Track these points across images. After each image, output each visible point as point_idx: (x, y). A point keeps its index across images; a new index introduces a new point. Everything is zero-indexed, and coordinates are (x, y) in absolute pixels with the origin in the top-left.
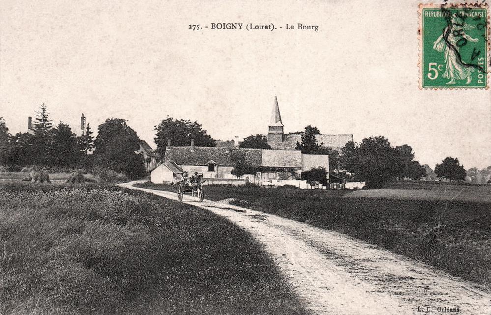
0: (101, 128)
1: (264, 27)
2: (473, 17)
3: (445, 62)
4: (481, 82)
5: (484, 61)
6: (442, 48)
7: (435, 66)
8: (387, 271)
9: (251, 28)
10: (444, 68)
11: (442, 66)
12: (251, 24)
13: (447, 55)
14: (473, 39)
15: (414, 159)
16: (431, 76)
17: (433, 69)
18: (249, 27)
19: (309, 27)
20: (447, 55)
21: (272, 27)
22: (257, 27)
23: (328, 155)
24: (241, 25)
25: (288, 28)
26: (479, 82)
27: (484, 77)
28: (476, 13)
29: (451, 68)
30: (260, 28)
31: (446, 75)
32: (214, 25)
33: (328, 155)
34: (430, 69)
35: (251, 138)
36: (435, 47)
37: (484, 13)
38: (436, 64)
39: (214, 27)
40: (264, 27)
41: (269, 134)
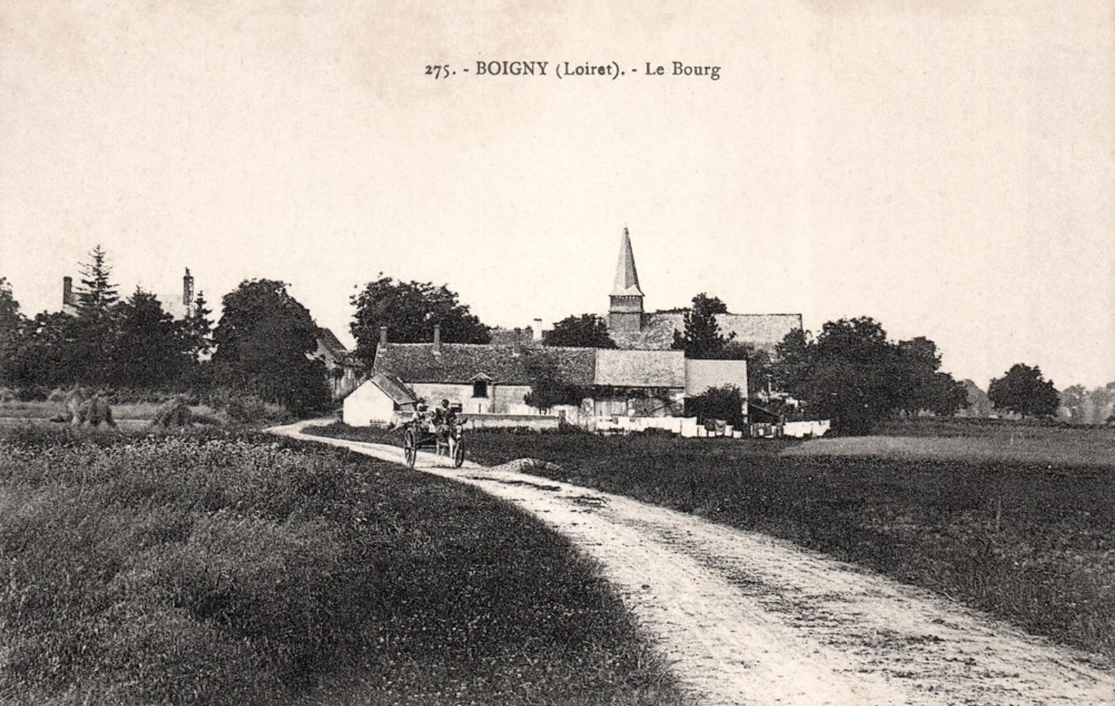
1: (596, 71)
9: (567, 73)
18: (562, 71)
19: (698, 71)
24: (543, 65)
30: (587, 73)
32: (482, 65)
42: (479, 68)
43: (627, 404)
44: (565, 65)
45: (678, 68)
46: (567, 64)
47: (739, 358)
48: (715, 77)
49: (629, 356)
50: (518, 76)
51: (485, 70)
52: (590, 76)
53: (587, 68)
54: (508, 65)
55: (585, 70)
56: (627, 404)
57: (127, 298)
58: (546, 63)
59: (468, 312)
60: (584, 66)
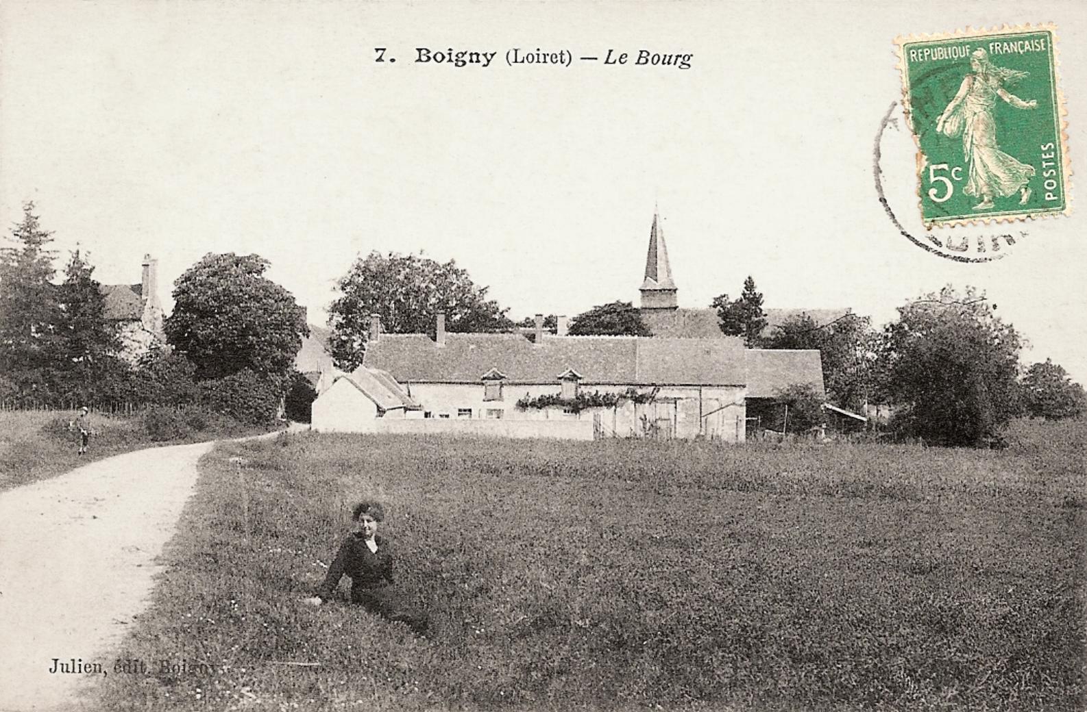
1: (548, 59)
2: (1021, 52)
3: (966, 160)
4: (1052, 198)
5: (1055, 150)
6: (955, 129)
7: (944, 169)
9: (516, 62)
10: (965, 175)
11: (960, 169)
13: (968, 145)
14: (1024, 103)
16: (935, 195)
17: (937, 179)
18: (512, 58)
19: (667, 60)
20: (968, 145)
21: (566, 57)
22: (532, 58)
26: (1047, 199)
27: (1058, 184)
28: (1005, 44)
29: (980, 171)
31: (971, 189)
32: (644, 54)
34: (933, 179)
36: (939, 129)
37: (1045, 42)
38: (945, 166)
41: (62, 664)
42: (640, 57)
44: (514, 52)
45: (644, 58)
46: (516, 50)
47: (812, 344)
48: (460, 64)
49: (792, 365)
51: (647, 60)
55: (536, 57)
58: (492, 55)
59: (741, 300)
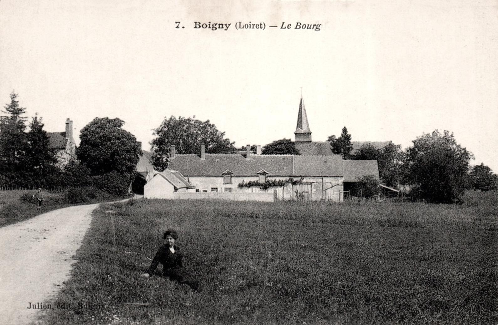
0: (85, 134)
1: (255, 26)
8: (248, 182)
9: (240, 28)
12: (240, 23)
15: (473, 163)
23: (375, 162)
24: (228, 26)
25: (241, 27)
30: (250, 28)
32: (299, 24)
33: (375, 162)
35: (281, 143)
39: (298, 27)
40: (255, 26)
43: (311, 187)
45: (299, 26)
50: (205, 29)
51: (300, 27)
52: (251, 29)
53: (250, 25)
54: (249, 27)
55: (249, 26)
56: (311, 187)
57: (6, 104)
58: (229, 25)
60: (248, 23)
